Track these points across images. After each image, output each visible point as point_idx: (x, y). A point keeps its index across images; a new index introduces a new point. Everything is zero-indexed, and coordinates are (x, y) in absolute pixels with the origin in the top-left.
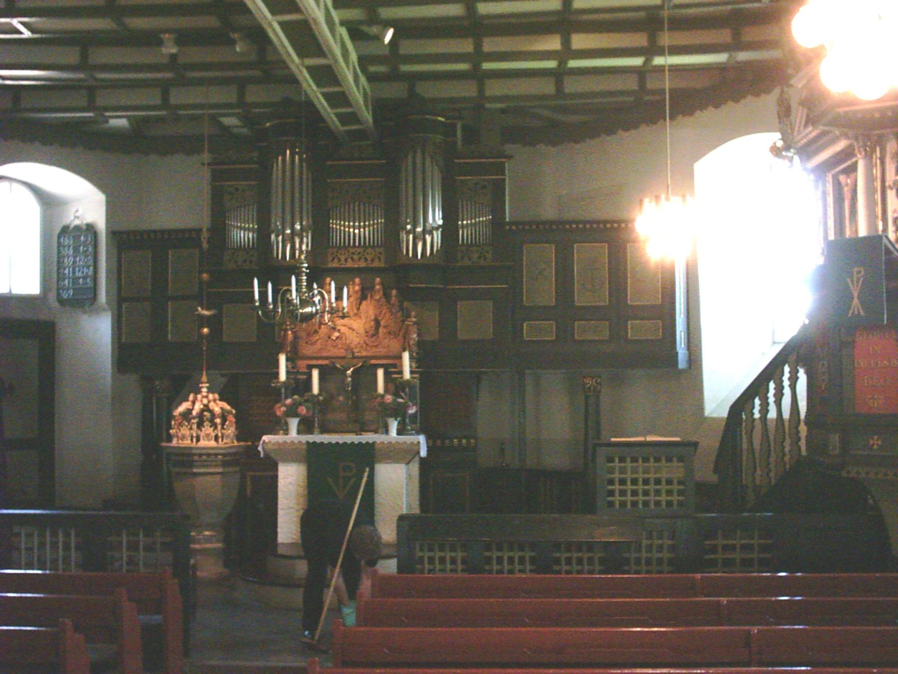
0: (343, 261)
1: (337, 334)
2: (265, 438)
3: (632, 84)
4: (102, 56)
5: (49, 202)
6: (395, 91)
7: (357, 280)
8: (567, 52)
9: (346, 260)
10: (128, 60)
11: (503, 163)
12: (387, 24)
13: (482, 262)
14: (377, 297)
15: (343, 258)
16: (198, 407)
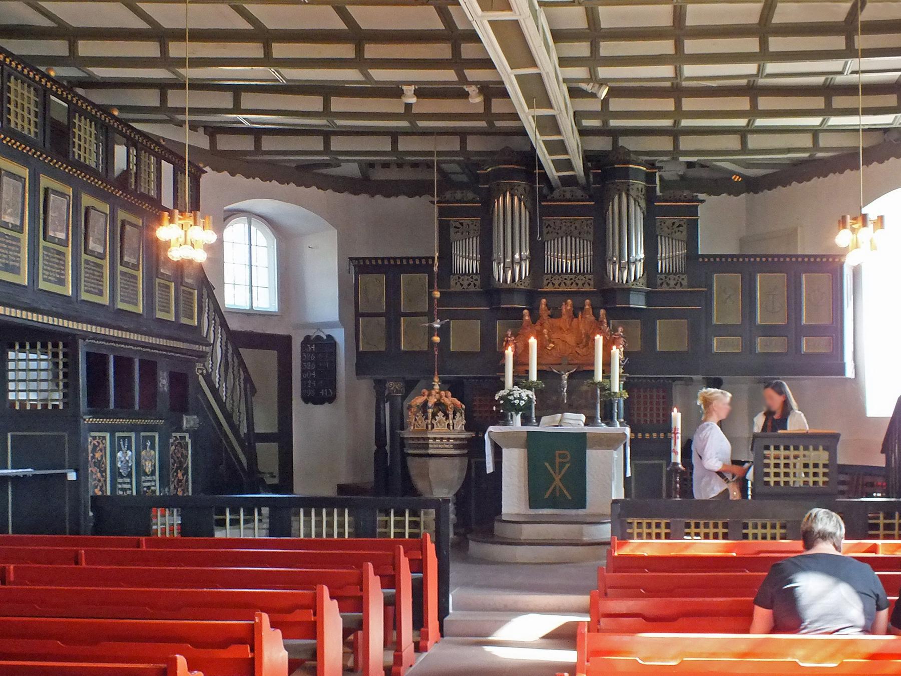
0: (557, 285)
2: (491, 428)
3: (806, 141)
4: (338, 104)
6: (601, 144)
8: (679, 113)
11: (697, 206)
12: (602, 83)
13: (678, 289)
15: (557, 283)
16: (432, 401)
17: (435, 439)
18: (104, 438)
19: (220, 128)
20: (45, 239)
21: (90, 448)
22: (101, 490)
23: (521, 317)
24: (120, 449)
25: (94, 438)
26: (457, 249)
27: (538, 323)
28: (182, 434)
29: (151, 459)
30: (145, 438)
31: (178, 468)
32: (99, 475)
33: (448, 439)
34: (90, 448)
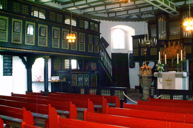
1: (171, 53)
5: (126, 32)
7: (175, 42)
9: (178, 38)
10: (101, 9)
14: (179, 45)
17: (143, 76)
18: (76, 75)
19: (112, 12)
20: (63, 40)
21: (72, 77)
22: (75, 85)
23: (164, 46)
24: (85, 77)
25: (73, 75)
26: (152, 32)
27: (168, 48)
28: (95, 75)
29: (87, 79)
30: (85, 75)
31: (93, 82)
32: (74, 82)
33: (146, 76)
34: (72, 77)
